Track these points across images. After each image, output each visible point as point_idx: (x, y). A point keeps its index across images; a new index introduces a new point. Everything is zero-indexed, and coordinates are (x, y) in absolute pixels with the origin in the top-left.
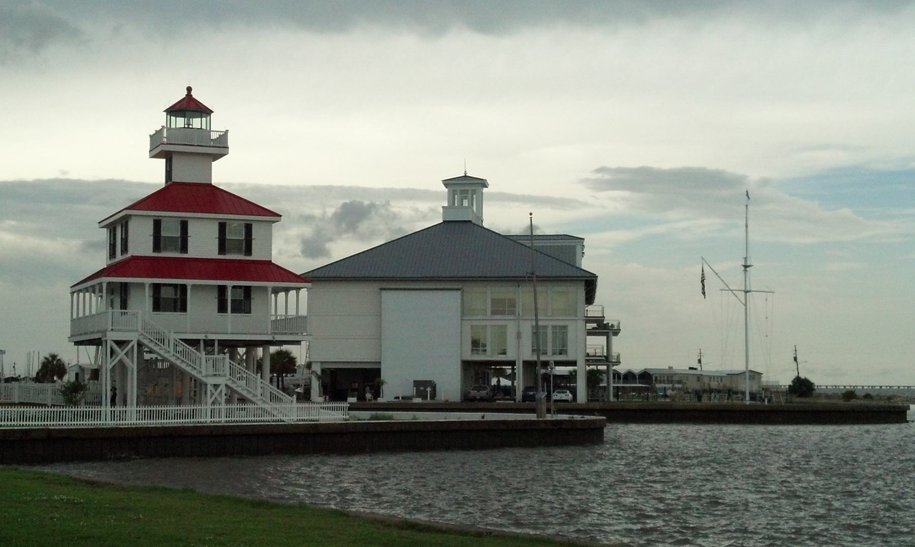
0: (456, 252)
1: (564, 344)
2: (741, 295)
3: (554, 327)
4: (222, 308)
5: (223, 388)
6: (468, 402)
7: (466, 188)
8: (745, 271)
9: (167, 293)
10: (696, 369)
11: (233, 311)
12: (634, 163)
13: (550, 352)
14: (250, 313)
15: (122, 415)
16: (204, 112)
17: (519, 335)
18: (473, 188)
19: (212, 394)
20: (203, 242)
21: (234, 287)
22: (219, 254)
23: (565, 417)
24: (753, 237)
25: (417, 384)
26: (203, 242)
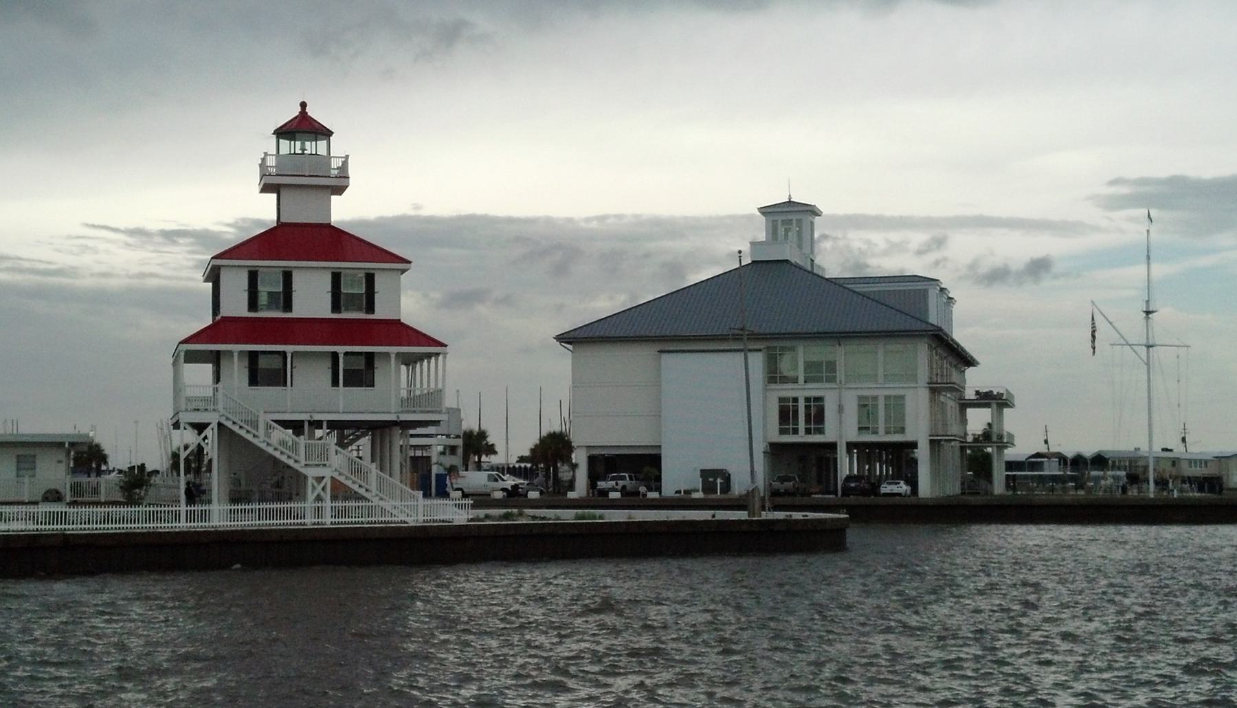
0: (773, 298)
1: (902, 418)
2: (1143, 351)
3: (887, 398)
4: (335, 382)
5: (327, 481)
6: (777, 498)
7: (790, 217)
8: (1147, 318)
9: (263, 363)
10: (1171, 450)
11: (345, 385)
12: (1162, 170)
13: (881, 430)
14: (371, 384)
15: (204, 516)
16: (324, 133)
17: (841, 409)
18: (799, 216)
19: (314, 488)
20: (312, 296)
21: (346, 354)
22: (333, 311)
23: (780, 515)
24: (1143, 268)
25: (705, 474)
26: (312, 296)
